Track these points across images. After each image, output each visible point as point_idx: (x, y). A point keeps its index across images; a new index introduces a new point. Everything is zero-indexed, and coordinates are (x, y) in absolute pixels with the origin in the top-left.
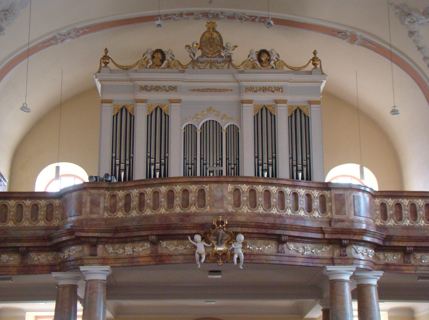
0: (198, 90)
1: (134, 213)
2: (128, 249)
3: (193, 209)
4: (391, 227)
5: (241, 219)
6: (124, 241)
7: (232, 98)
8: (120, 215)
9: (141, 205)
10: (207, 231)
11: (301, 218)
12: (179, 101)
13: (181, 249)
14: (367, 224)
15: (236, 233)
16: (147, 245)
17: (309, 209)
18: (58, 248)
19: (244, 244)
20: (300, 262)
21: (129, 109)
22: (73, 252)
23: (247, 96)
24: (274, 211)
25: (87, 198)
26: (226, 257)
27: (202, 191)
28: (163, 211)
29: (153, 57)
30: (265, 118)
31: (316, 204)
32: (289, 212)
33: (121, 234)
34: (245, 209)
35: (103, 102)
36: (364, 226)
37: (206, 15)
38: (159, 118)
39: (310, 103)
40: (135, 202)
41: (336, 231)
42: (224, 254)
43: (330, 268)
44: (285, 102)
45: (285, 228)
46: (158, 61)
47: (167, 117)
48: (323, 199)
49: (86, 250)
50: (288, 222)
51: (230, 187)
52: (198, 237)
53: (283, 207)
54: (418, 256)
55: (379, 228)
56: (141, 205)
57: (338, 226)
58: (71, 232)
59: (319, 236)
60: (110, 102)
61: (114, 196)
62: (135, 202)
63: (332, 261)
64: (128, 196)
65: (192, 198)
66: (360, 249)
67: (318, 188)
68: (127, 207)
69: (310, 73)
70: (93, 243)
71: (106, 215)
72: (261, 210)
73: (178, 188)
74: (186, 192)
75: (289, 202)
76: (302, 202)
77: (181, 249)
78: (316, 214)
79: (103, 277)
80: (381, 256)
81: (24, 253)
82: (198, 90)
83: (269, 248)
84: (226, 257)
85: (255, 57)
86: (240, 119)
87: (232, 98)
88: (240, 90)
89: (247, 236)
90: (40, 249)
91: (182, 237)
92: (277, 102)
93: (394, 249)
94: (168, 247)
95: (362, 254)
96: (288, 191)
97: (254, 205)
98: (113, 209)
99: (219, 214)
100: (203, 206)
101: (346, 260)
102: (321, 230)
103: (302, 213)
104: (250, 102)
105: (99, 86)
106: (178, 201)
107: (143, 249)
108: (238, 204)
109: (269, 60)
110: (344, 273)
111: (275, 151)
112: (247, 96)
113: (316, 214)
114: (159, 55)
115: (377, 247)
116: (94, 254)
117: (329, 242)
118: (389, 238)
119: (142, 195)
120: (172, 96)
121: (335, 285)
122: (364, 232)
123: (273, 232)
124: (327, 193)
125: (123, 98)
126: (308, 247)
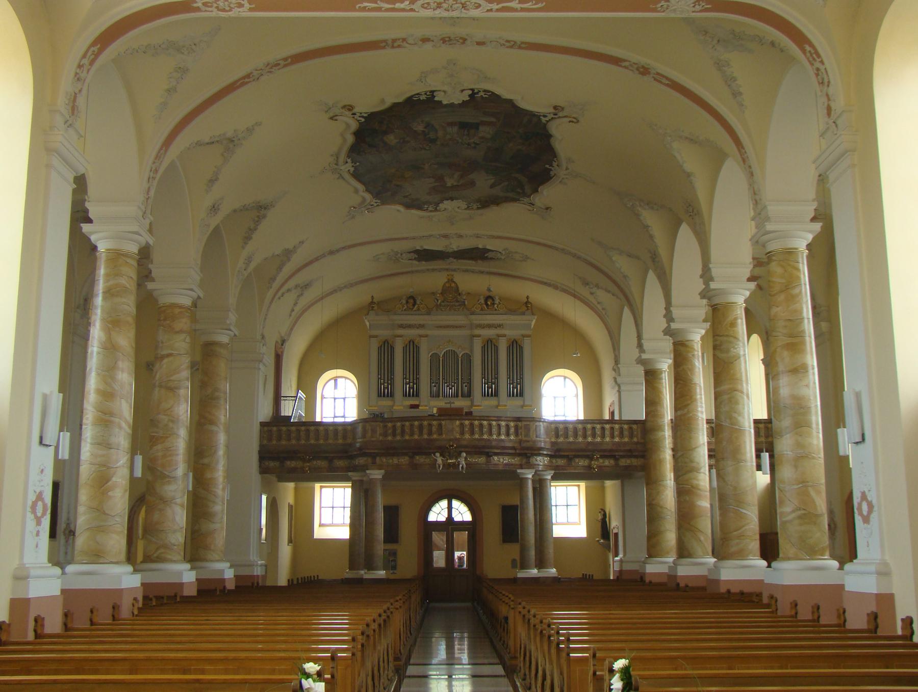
0: (441, 327)
1: (398, 438)
2: (396, 460)
3: (435, 436)
4: (561, 443)
5: (464, 443)
6: (393, 455)
7: (465, 332)
8: (390, 438)
9: (403, 432)
10: (443, 451)
11: (502, 440)
12: (426, 336)
13: (428, 461)
14: (545, 442)
15: (461, 452)
16: (407, 458)
17: (508, 434)
18: (351, 457)
19: (466, 458)
20: (501, 468)
21: (390, 342)
22: (361, 461)
23: (477, 332)
24: (485, 437)
25: (368, 427)
26: (455, 466)
27: (440, 425)
28: (416, 437)
29: (407, 302)
30: (490, 346)
31: (512, 430)
32: (495, 437)
33: (390, 450)
34: (467, 436)
35: (371, 337)
36: (543, 445)
37: (447, 270)
38: (412, 348)
39: (524, 336)
40: (399, 431)
41: (523, 448)
42: (454, 464)
43: (519, 471)
44: (504, 336)
45: (492, 447)
46: (410, 305)
47: (418, 348)
48: (516, 427)
49: (370, 460)
50: (494, 443)
51: (458, 422)
52: (438, 454)
53: (491, 434)
54: (577, 460)
55: (553, 444)
56: (403, 432)
57: (524, 445)
58: (360, 449)
59: (512, 451)
60: (376, 337)
61: (386, 426)
62: (399, 431)
63: (521, 467)
64: (394, 426)
65: (434, 429)
66: (539, 458)
67: (514, 421)
68: (394, 435)
69: (523, 314)
70: (373, 456)
71: (381, 438)
72: (477, 436)
73: (425, 423)
74: (430, 425)
75: (494, 430)
76: (503, 430)
77: (428, 461)
78: (512, 437)
79: (381, 477)
80: (554, 461)
81: (330, 460)
82: (441, 327)
83: (482, 460)
84: (455, 466)
85: (483, 302)
86: (472, 351)
87: (465, 332)
88: (472, 326)
89: (467, 453)
90: (340, 458)
91: (428, 454)
92: (499, 336)
93: (561, 457)
94: (420, 459)
95: (541, 461)
96: (494, 423)
97: (472, 433)
98: (385, 434)
99: (450, 440)
100: (441, 434)
101: (530, 466)
102: (513, 448)
103: (503, 437)
104: (479, 336)
105: (368, 324)
106: (425, 431)
107: (404, 460)
108: (462, 433)
109: (494, 304)
110: (529, 474)
111: (497, 373)
112: (477, 332)
113: (512, 437)
114: (411, 301)
115: (551, 456)
116: (374, 463)
117: (520, 455)
118: (559, 450)
119: (403, 426)
120: (421, 332)
121: (522, 481)
122: (541, 449)
123: (484, 449)
124: (520, 424)
125: (385, 333)
126: (506, 458)
